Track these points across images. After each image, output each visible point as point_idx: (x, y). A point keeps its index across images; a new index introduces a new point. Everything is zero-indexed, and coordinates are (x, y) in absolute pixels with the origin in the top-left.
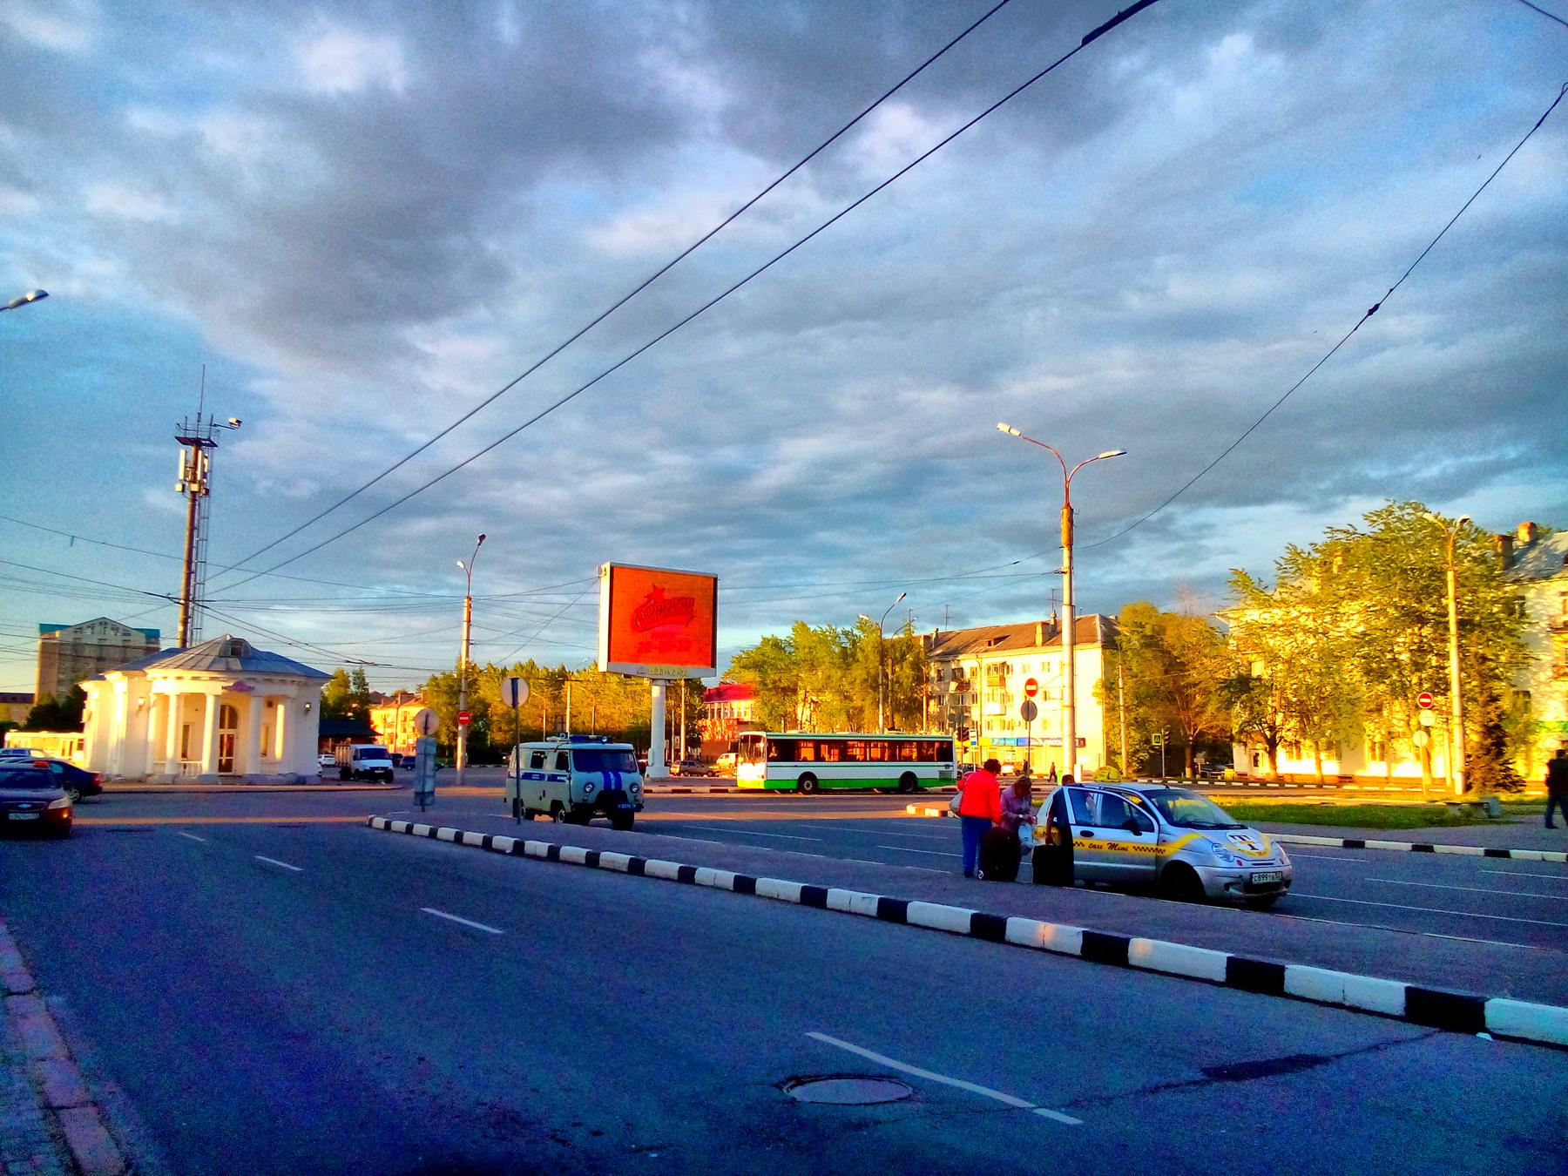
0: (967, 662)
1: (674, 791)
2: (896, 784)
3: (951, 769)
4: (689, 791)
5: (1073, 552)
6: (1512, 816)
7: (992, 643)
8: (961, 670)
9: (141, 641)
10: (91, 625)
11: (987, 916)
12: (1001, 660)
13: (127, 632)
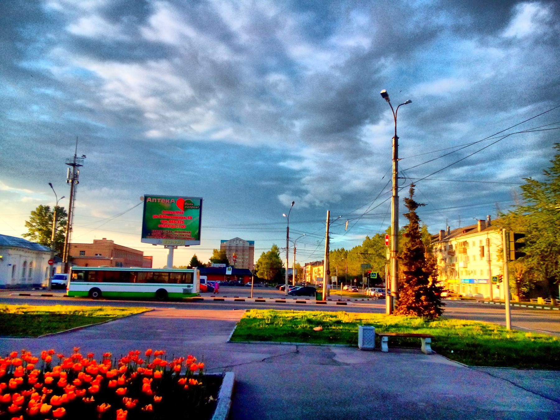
0: (454, 242)
1: (43, 296)
2: (153, 296)
3: (191, 288)
4: (51, 296)
5: (134, 209)
6: (472, 324)
7: (465, 232)
8: (452, 245)
9: (247, 245)
10: (233, 240)
11: (214, 413)
12: (464, 240)
13: (244, 241)
